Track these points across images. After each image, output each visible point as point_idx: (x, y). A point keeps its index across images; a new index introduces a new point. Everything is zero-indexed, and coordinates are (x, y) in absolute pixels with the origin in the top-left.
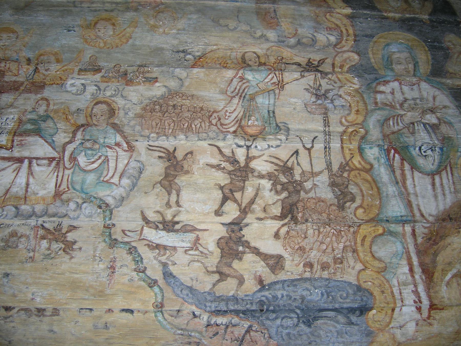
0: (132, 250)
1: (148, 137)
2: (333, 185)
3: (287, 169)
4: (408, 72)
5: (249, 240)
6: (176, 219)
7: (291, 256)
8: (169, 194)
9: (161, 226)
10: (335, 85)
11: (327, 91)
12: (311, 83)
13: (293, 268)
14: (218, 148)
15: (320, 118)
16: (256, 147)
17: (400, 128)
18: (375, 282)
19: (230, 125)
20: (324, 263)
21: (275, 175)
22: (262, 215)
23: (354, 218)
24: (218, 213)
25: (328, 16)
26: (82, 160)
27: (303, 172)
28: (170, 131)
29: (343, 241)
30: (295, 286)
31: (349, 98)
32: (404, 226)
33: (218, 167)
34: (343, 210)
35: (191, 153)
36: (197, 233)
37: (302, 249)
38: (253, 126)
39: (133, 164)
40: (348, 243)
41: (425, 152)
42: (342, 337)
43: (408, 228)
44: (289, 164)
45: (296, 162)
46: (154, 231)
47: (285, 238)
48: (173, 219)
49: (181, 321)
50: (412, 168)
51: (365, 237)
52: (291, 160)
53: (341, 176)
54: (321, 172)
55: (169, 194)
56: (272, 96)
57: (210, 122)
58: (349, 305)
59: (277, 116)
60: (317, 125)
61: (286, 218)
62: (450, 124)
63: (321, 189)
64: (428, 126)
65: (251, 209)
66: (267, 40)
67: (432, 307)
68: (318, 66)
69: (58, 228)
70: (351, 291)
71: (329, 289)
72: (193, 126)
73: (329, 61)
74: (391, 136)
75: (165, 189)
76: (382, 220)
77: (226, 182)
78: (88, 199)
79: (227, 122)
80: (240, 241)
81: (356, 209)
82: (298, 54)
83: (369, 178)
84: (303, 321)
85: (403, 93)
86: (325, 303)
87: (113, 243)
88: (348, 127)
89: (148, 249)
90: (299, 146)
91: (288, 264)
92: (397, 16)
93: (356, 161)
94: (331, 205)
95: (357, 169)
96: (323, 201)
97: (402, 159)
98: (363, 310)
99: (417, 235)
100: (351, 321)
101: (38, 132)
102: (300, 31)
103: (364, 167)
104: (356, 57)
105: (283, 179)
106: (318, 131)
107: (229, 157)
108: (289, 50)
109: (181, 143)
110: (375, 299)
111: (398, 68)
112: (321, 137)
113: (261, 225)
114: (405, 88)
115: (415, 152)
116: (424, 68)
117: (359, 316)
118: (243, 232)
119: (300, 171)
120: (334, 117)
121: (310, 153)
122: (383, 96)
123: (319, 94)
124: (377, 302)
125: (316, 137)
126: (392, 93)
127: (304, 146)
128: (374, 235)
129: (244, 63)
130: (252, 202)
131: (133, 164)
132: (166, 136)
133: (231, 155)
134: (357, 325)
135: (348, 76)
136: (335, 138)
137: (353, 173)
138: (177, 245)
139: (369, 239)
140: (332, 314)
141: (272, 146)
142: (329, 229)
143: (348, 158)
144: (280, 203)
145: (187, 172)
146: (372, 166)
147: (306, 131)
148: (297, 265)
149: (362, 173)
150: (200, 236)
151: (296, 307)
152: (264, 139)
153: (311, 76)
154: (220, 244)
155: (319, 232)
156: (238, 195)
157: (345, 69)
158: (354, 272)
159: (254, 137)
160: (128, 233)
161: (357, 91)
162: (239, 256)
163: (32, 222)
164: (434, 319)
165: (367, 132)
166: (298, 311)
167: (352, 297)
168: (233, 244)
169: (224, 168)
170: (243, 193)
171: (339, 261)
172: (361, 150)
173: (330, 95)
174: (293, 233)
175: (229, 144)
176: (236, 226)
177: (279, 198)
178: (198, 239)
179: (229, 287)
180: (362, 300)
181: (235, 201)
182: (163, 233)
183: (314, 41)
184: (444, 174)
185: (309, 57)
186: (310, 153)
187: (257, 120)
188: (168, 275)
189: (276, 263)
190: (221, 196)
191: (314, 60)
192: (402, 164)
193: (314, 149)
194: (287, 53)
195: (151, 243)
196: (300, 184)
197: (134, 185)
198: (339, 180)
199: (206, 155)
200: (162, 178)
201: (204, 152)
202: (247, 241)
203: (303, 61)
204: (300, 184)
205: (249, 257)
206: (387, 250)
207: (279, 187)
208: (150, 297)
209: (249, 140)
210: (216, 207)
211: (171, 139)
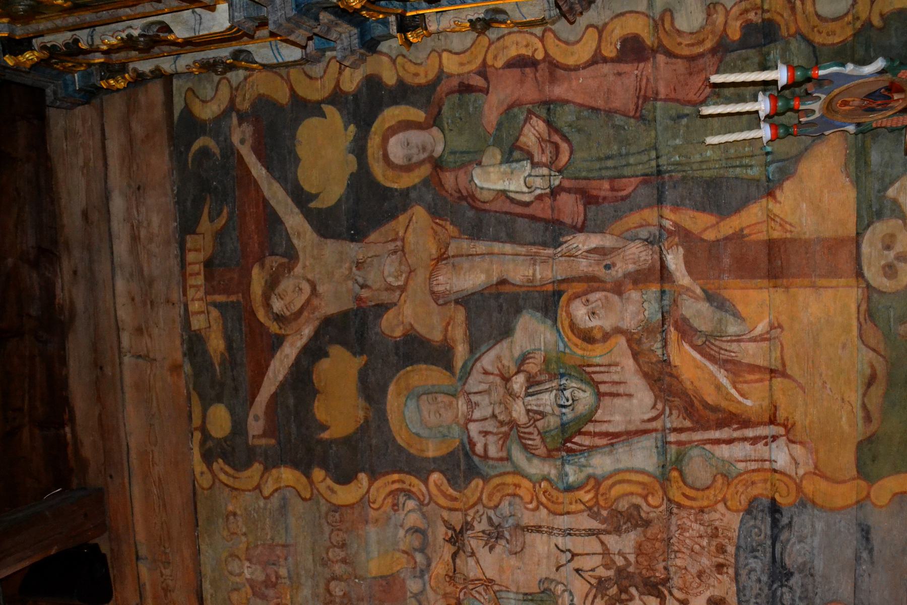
2: (618, 531)
7: (709, 588)
10: (481, 512)
17: (536, 433)
18: (741, 490)
20: (717, 550)
23: (661, 509)
25: (375, 506)
29: (689, 523)
30: (744, 587)
32: (670, 443)
37: (700, 574)
40: (692, 517)
41: (568, 400)
42: (806, 537)
43: (672, 437)
45: (590, 573)
47: (687, 593)
50: (591, 421)
51: (684, 495)
52: (589, 579)
54: (602, 543)
56: (504, 595)
58: (769, 528)
59: (531, 591)
60: (540, 544)
61: (663, 592)
64: (530, 390)
66: (423, 591)
67: (772, 421)
68: (455, 530)
70: (752, 523)
76: (663, 474)
81: (649, 505)
82: (439, 555)
84: (786, 581)
86: (765, 556)
88: (540, 503)
91: (717, 592)
94: (645, 536)
95: (596, 496)
97: (580, 433)
98: (775, 509)
99: (680, 426)
100: (787, 525)
103: (593, 487)
108: (433, 565)
110: (762, 495)
115: (569, 415)
117: (781, 514)
120: (528, 519)
121: (577, 555)
123: (494, 535)
124: (765, 492)
125: (556, 546)
128: (681, 484)
134: (792, 518)
137: (602, 503)
139: (688, 491)
140: (778, 547)
143: (582, 507)
144: (645, 598)
146: (589, 477)
148: (720, 582)
149: (602, 490)
151: (769, 590)
153: (471, 543)
155: (679, 551)
158: (728, 515)
164: (787, 419)
166: (775, 586)
167: (758, 523)
172: (569, 489)
177: (637, 598)
180: (762, 511)
183: (415, 530)
185: (442, 541)
186: (577, 555)
191: (446, 534)
193: (572, 549)
194: (439, 568)
196: (620, 571)
203: (447, 551)
204: (620, 571)
206: (698, 469)
207: (624, 596)
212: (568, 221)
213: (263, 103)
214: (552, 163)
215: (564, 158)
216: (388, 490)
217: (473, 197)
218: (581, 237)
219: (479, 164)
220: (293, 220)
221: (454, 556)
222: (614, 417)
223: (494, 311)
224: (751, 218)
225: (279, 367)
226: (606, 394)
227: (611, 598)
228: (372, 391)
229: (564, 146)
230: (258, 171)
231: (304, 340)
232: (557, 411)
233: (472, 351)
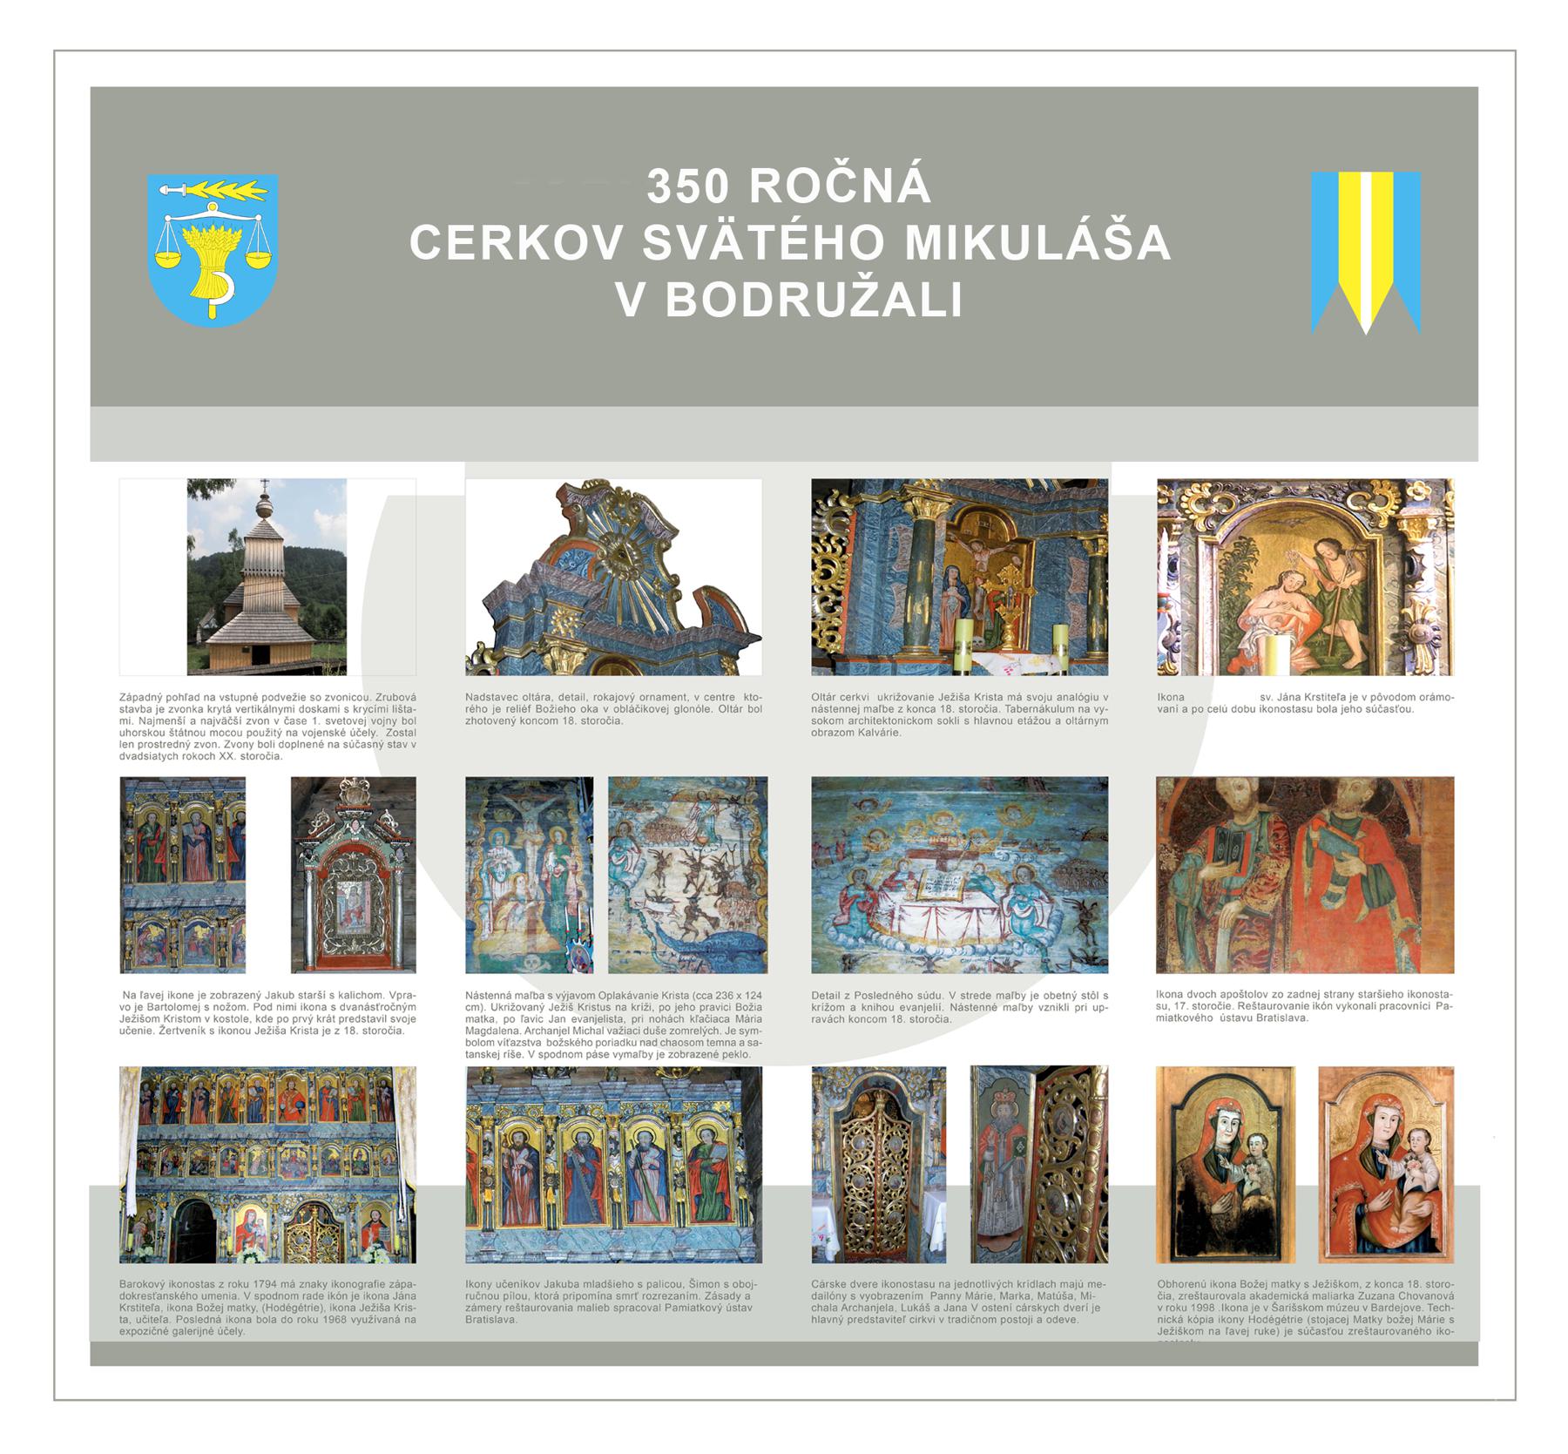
0: (640, 914)
3: (720, 864)
13: (724, 926)
24: (685, 891)
26: (1016, 909)
49: (665, 959)
60: (737, 837)
63: (739, 877)
69: (1007, 963)
71: (744, 937)
78: (1028, 939)
80: (697, 909)
87: (630, 910)
101: (980, 889)
109: (665, 848)
120: (745, 832)
123: (738, 818)
129: (698, 799)
159: (704, 844)
162: (695, 918)
163: (986, 958)
168: (693, 912)
171: (748, 921)
175: (690, 849)
176: (694, 899)
179: (690, 938)
188: (659, 930)
189: (715, 922)
194: (721, 792)
197: (1059, 929)
199: (679, 856)
201: (678, 854)
205: (701, 919)
208: (649, 943)
220: (542, 807)
222: (497, 886)
223: (520, 855)
224: (541, 926)
225: (509, 800)
228: (504, 824)
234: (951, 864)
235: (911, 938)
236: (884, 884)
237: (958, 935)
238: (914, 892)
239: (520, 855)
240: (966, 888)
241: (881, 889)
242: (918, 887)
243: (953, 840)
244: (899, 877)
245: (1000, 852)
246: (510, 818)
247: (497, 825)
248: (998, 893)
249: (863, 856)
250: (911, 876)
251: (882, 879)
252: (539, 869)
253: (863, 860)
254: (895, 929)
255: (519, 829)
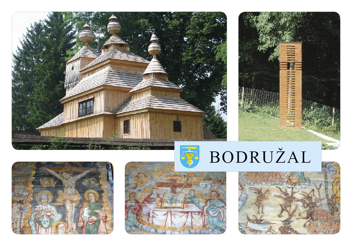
1: (250, 184)
2: (329, 204)
4: (46, 202)
5: (293, 228)
6: (262, 219)
8: (259, 208)
9: (255, 222)
11: (23, 208)
12: (19, 206)
14: (279, 188)
15: (20, 215)
16: (296, 188)
19: (285, 179)
21: (304, 200)
22: (298, 217)
24: (280, 216)
27: (316, 198)
28: (259, 181)
31: (28, 210)
33: (280, 197)
34: (333, 215)
35: (268, 190)
36: (271, 224)
38: (295, 179)
39: (243, 195)
44: (310, 195)
46: (252, 224)
48: (260, 219)
52: (311, 194)
53: (23, 229)
55: (259, 208)
57: (276, 178)
62: (54, 215)
65: (294, 215)
72: (269, 179)
73: (25, 200)
74: (37, 219)
75: (257, 206)
77: (283, 203)
79: (283, 177)
83: (30, 229)
85: (42, 208)
88: (335, 180)
89: (250, 232)
90: (314, 188)
92: (46, 186)
93: (27, 225)
96: (324, 211)
97: (39, 225)
101: (193, 202)
102: (19, 192)
104: (32, 198)
105: (307, 202)
106: (322, 181)
107: (284, 192)
109: (264, 186)
111: (43, 201)
112: (324, 183)
113: (298, 221)
114: (43, 206)
115: (42, 223)
116: (50, 200)
118: (290, 224)
119: (315, 198)
120: (23, 215)
121: (319, 190)
122: (37, 209)
126: (40, 208)
127: (316, 188)
130: (294, 211)
131: (243, 195)
132: (257, 183)
133: (285, 191)
135: (29, 204)
136: (330, 184)
137: (26, 228)
138: (262, 229)
141: (303, 188)
142: (327, 223)
145: (266, 199)
146: (31, 226)
147: (317, 181)
150: (272, 226)
152: (299, 185)
154: (280, 229)
156: (288, 209)
157: (29, 202)
159: (295, 184)
160: (242, 225)
161: (30, 208)
165: (31, 218)
169: (282, 197)
170: (290, 207)
172: (29, 222)
173: (23, 209)
174: (312, 225)
176: (287, 222)
177: (306, 209)
178: (271, 227)
181: (287, 211)
182: (257, 225)
183: (22, 195)
184: (49, 228)
186: (319, 190)
187: (296, 176)
190: (281, 209)
192: (39, 226)
195: (251, 229)
196: (315, 204)
198: (331, 202)
200: (255, 201)
202: (292, 228)
203: (18, 200)
204: (315, 204)
207: (306, 205)
209: (293, 185)
210: (279, 214)
211: (260, 185)
212: (79, 223)
213: (99, 174)
214: (89, 221)
215: (90, 223)
216: (30, 190)
217: (83, 207)
218: (75, 226)
219: (89, 209)
220: (79, 177)
221: (17, 201)
223: (61, 209)
226: (46, 229)
227: (305, 201)
228: (48, 188)
229: (91, 224)
230: (88, 172)
231: (58, 177)
232: (43, 221)
233: (56, 206)
234: (178, 190)
235: (158, 227)
236: (145, 200)
237: (181, 225)
238: (160, 204)
239: (61, 209)
240: (185, 202)
241: (143, 203)
242: (162, 201)
243: (179, 178)
244: (152, 196)
245: (202, 184)
246: (53, 184)
247: (42, 188)
248: (202, 204)
249: (134, 186)
250: (158, 195)
251: (144, 197)
252: (77, 219)
253: (135, 188)
254: (151, 222)
255: (60, 192)
